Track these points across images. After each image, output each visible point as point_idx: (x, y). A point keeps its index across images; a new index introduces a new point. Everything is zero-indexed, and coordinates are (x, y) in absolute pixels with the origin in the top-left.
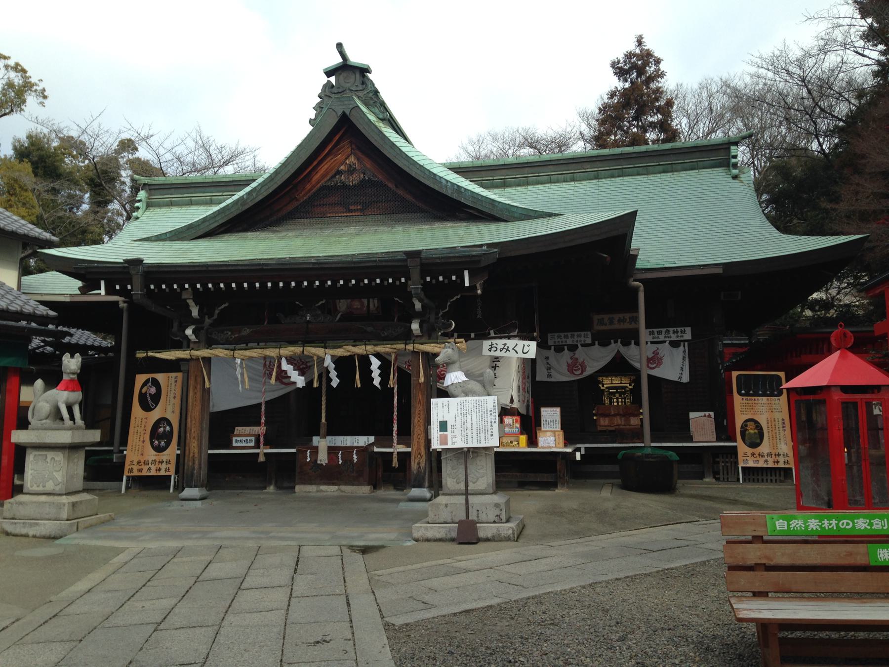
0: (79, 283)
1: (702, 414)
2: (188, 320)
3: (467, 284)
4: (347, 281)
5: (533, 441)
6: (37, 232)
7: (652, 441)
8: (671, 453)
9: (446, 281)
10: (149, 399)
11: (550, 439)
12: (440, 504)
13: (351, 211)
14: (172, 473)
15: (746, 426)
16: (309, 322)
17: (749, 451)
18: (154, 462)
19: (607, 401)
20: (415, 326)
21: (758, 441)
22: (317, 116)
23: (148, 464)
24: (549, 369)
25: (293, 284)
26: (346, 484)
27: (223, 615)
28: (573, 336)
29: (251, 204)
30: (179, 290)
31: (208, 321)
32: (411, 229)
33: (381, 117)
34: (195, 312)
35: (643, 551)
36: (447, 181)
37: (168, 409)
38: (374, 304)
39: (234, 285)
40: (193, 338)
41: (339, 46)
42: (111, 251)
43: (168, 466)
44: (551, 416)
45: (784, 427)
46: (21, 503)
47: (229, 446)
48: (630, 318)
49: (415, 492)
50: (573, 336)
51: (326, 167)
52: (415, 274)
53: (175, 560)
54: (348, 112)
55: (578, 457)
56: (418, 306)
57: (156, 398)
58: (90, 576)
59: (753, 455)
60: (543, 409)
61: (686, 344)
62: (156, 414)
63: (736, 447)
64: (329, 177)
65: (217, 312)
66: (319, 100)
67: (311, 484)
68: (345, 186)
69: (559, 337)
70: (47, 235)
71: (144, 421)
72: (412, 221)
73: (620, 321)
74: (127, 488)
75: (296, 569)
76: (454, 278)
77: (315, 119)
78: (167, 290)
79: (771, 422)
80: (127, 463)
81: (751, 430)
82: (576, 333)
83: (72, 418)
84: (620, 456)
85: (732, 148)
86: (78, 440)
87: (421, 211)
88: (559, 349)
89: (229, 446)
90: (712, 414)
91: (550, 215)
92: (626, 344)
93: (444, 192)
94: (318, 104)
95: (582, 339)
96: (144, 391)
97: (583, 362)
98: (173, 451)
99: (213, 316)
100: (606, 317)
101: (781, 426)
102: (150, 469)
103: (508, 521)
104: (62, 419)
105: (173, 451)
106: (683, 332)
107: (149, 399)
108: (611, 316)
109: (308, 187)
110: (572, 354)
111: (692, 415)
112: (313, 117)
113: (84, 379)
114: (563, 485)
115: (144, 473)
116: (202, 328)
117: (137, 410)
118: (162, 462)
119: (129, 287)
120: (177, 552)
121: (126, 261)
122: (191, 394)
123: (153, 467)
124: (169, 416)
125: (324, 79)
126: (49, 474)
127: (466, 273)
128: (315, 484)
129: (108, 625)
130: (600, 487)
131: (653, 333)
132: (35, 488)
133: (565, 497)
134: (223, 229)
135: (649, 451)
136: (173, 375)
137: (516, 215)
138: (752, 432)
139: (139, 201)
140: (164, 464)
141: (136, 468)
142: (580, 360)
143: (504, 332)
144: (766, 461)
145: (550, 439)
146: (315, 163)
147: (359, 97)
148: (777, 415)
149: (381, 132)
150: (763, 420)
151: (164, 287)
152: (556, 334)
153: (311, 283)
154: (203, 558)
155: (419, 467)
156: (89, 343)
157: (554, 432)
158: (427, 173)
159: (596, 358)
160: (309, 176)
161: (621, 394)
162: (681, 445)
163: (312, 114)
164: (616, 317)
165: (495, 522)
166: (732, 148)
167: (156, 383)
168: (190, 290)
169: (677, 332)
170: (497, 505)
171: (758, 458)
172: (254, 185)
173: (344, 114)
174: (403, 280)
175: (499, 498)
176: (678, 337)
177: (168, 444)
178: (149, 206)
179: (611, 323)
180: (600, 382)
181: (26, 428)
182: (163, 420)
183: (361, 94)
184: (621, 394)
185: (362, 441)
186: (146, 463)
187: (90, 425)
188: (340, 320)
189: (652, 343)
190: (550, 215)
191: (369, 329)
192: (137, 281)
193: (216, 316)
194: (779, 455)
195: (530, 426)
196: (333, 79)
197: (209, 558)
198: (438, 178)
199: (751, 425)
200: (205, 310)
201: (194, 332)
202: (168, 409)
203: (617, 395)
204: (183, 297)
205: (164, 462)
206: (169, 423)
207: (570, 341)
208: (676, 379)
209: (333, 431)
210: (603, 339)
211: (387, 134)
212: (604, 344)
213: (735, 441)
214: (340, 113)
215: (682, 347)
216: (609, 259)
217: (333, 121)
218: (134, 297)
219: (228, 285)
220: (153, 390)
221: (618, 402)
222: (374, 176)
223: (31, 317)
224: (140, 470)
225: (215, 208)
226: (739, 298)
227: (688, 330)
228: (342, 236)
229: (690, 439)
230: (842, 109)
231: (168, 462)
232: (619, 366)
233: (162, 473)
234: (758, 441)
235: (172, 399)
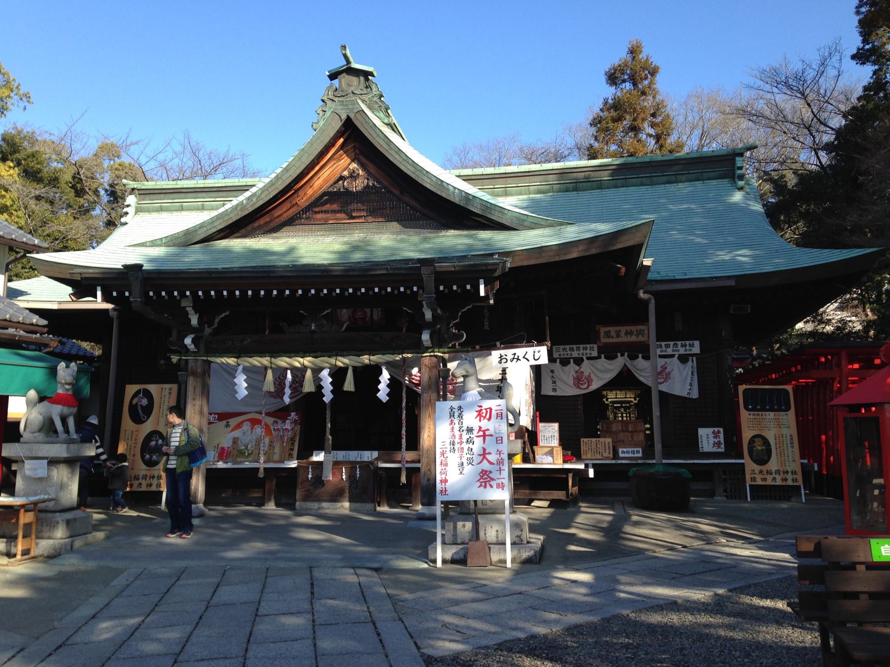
0: (69, 290)
3: (482, 293)
4: (331, 291)
6: (26, 238)
8: (683, 470)
9: (446, 291)
13: (354, 218)
15: (754, 442)
16: (313, 332)
17: (757, 468)
19: (611, 416)
20: (426, 337)
21: (766, 458)
24: (554, 382)
25: (275, 292)
27: (245, 646)
28: (578, 349)
29: (251, 210)
30: (178, 298)
31: (208, 331)
33: (386, 121)
34: (194, 321)
35: (674, 575)
36: (455, 188)
38: (377, 314)
39: (213, 293)
40: (192, 347)
42: (113, 253)
44: (549, 433)
45: (792, 443)
50: (578, 349)
51: (328, 172)
53: (181, 582)
54: (352, 116)
55: (591, 474)
56: (428, 315)
57: (148, 410)
59: (761, 472)
61: (694, 358)
63: (743, 464)
65: (217, 320)
68: (347, 193)
69: (564, 349)
71: (135, 433)
73: (627, 333)
75: (312, 593)
76: (468, 287)
78: (167, 298)
79: (779, 437)
81: (759, 446)
82: (582, 346)
83: (67, 431)
84: (631, 473)
85: (738, 159)
86: (73, 454)
88: (565, 362)
90: (721, 430)
92: (633, 357)
93: (452, 199)
95: (588, 351)
96: (134, 402)
99: (213, 324)
100: (613, 330)
101: (789, 442)
102: (140, 484)
104: (56, 431)
106: (692, 346)
108: (618, 328)
110: (577, 368)
117: (127, 422)
118: (153, 477)
119: (127, 294)
120: (180, 574)
121: (126, 267)
123: (144, 483)
129: (122, 656)
131: (661, 346)
134: (222, 234)
136: (167, 386)
137: (526, 224)
138: (760, 448)
139: (128, 206)
142: (586, 374)
143: (511, 342)
144: (774, 479)
146: (317, 168)
147: (363, 101)
148: (785, 431)
150: (770, 436)
151: (163, 294)
152: (562, 347)
153: (306, 291)
154: (209, 580)
158: (434, 179)
159: (600, 372)
161: (625, 408)
162: (692, 462)
164: (623, 329)
166: (738, 159)
167: (148, 394)
169: (685, 346)
172: (254, 190)
173: (349, 119)
176: (686, 350)
178: (138, 211)
179: (618, 336)
180: (604, 396)
183: (364, 97)
184: (625, 408)
185: (369, 456)
188: (345, 331)
189: (660, 356)
192: (137, 287)
193: (216, 325)
194: (787, 472)
197: (215, 580)
198: (445, 185)
199: (758, 442)
201: (193, 341)
203: (622, 410)
204: (182, 305)
207: (575, 354)
208: (685, 394)
210: (609, 352)
212: (611, 357)
213: (742, 458)
214: (344, 117)
215: (690, 363)
216: (623, 270)
218: (133, 305)
219: (231, 293)
220: (145, 402)
221: (622, 417)
225: (214, 213)
226: (749, 311)
227: (697, 343)
230: (837, 122)
232: (625, 380)
234: (766, 458)
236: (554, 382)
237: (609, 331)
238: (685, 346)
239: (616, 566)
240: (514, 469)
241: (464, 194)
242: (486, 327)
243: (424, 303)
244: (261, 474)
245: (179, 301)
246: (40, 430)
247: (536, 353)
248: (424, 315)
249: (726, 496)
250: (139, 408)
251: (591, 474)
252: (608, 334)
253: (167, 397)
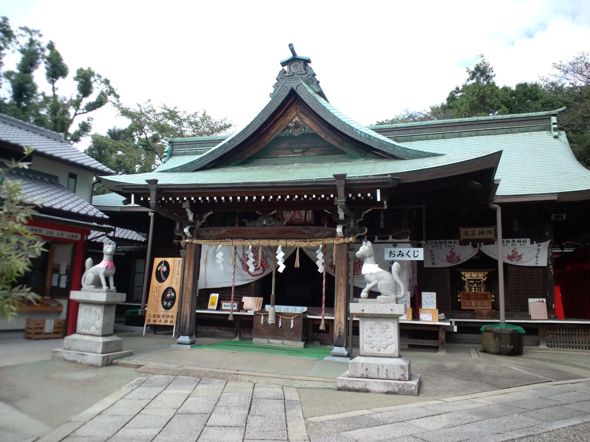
1: (538, 300)
2: (185, 222)
3: (379, 199)
5: (416, 316)
7: (506, 319)
10: (162, 275)
11: (429, 315)
12: (357, 363)
13: (295, 153)
14: (174, 324)
16: (265, 225)
18: (163, 316)
19: (467, 289)
20: (339, 230)
22: (275, 91)
23: (159, 317)
26: (287, 339)
29: (231, 148)
31: (199, 223)
32: (335, 165)
33: (317, 91)
34: (191, 217)
36: (361, 132)
37: (174, 281)
38: (310, 215)
40: (189, 234)
41: (291, 45)
43: (172, 319)
44: (429, 299)
46: (75, 340)
47: (206, 308)
48: (487, 231)
49: (337, 350)
52: (341, 192)
54: (295, 89)
56: (341, 215)
57: (166, 274)
58: (105, 399)
60: (423, 293)
62: (166, 284)
64: (281, 131)
65: (205, 217)
66: (277, 81)
67: (263, 338)
68: (291, 137)
70: (108, 170)
71: (158, 288)
74: (147, 331)
76: (369, 195)
77: (273, 94)
80: (147, 315)
82: (448, 241)
87: (342, 153)
89: (206, 308)
90: (544, 300)
91: (435, 155)
94: (277, 83)
96: (159, 269)
97: (521, 256)
98: (174, 311)
100: (470, 230)
102: (161, 320)
103: (410, 379)
105: (174, 311)
107: (162, 275)
109: (268, 137)
111: (530, 300)
112: (272, 92)
113: (116, 258)
114: (443, 348)
115: (158, 323)
116: (195, 228)
118: (168, 316)
119: (149, 199)
122: (186, 272)
125: (280, 68)
126: (91, 320)
127: (378, 192)
128: (266, 338)
130: (468, 351)
132: (84, 331)
133: (442, 357)
135: (504, 326)
136: (177, 259)
137: (410, 155)
140: (170, 318)
141: (152, 319)
145: (429, 315)
149: (317, 100)
152: (434, 241)
155: (340, 332)
156: (134, 239)
157: (432, 310)
160: (267, 132)
163: (272, 90)
165: (400, 380)
167: (166, 264)
168: (188, 201)
169: (520, 242)
170: (402, 367)
171: (156, 319)
174: (332, 196)
175: (401, 362)
177: (172, 305)
180: (462, 275)
181: (80, 290)
182: (170, 289)
183: (304, 76)
184: (477, 284)
185: (300, 310)
186: (158, 316)
187: (119, 290)
188: (286, 225)
190: (435, 155)
191: (307, 232)
195: (416, 305)
196: (286, 68)
197: (188, 392)
200: (197, 216)
202: (174, 281)
203: (475, 285)
204: (184, 207)
205: (168, 317)
206: (174, 291)
209: (279, 302)
211: (320, 102)
217: (285, 94)
220: (165, 269)
222: (311, 129)
223: (94, 219)
224: (155, 321)
226: (565, 218)
228: (289, 169)
229: (529, 317)
233: (168, 324)
235: (176, 275)
236: (433, 259)
237: (467, 231)
238: (520, 242)
239: (476, 400)
240: (400, 323)
241: (367, 136)
242: (382, 226)
243: (338, 206)
244: (230, 318)
245: (181, 204)
246: (92, 284)
247: (416, 253)
248: (338, 215)
249: (548, 346)
250: (162, 272)
251: (455, 329)
252: (466, 233)
253: (177, 265)
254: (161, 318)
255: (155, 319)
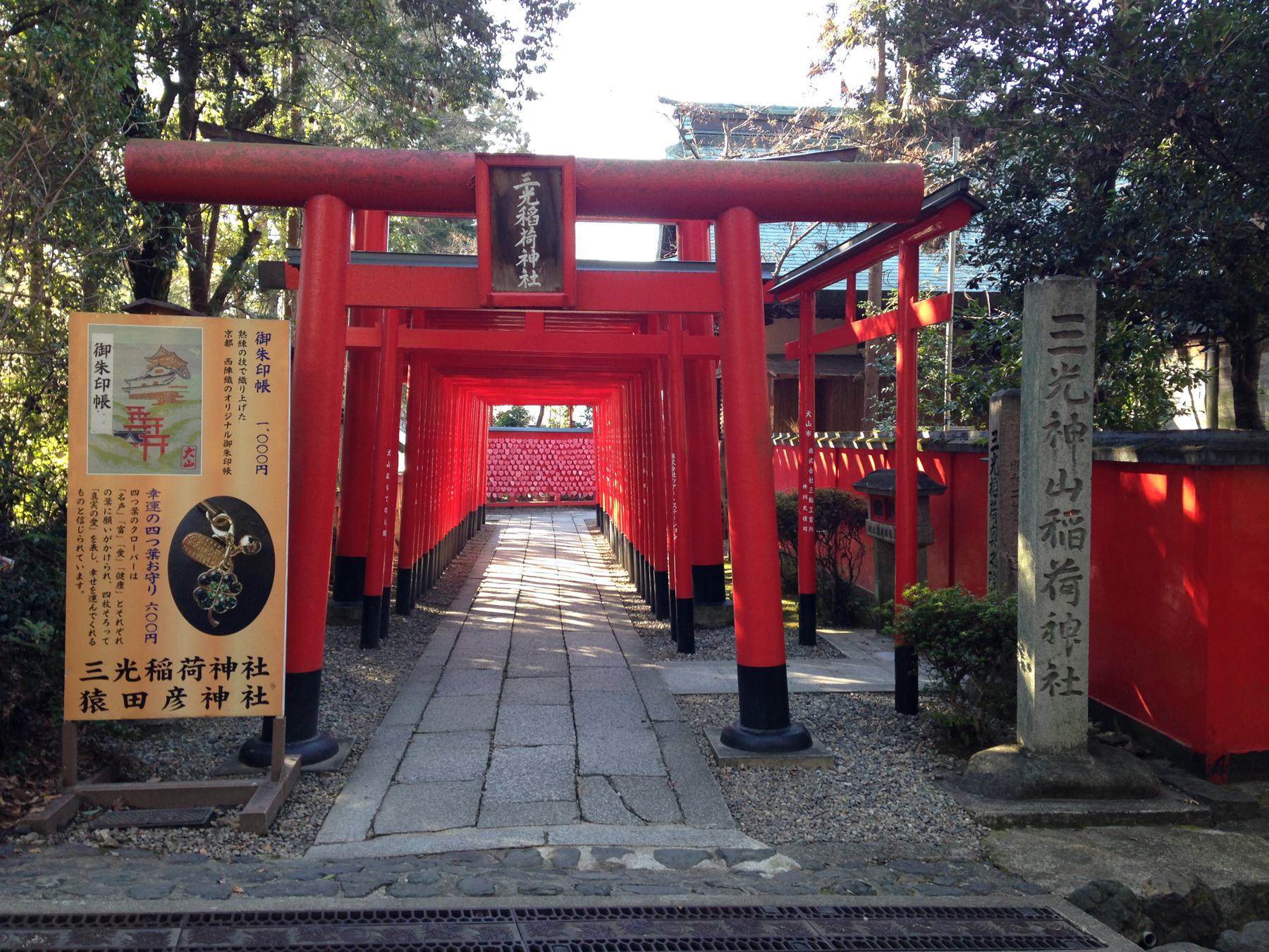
14: (815, 320)
18: (194, 667)
43: (256, 681)
72: (1091, 593)
102: (177, 694)
118: (230, 667)
124: (245, 487)
140: (238, 675)
141: (114, 691)
171: (145, 685)
186: (158, 670)
224: (138, 700)
231: (256, 667)
254: (177, 681)
255: (132, 688)
